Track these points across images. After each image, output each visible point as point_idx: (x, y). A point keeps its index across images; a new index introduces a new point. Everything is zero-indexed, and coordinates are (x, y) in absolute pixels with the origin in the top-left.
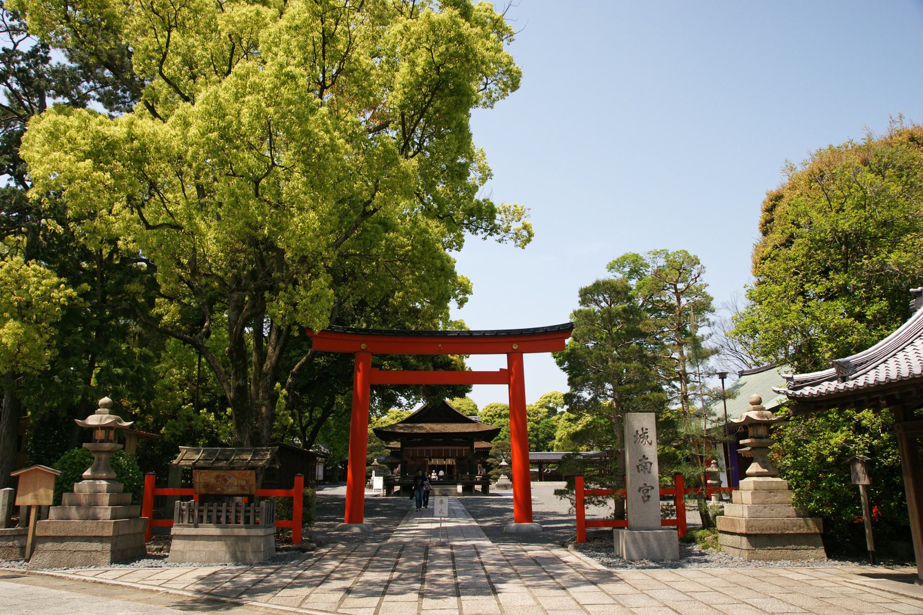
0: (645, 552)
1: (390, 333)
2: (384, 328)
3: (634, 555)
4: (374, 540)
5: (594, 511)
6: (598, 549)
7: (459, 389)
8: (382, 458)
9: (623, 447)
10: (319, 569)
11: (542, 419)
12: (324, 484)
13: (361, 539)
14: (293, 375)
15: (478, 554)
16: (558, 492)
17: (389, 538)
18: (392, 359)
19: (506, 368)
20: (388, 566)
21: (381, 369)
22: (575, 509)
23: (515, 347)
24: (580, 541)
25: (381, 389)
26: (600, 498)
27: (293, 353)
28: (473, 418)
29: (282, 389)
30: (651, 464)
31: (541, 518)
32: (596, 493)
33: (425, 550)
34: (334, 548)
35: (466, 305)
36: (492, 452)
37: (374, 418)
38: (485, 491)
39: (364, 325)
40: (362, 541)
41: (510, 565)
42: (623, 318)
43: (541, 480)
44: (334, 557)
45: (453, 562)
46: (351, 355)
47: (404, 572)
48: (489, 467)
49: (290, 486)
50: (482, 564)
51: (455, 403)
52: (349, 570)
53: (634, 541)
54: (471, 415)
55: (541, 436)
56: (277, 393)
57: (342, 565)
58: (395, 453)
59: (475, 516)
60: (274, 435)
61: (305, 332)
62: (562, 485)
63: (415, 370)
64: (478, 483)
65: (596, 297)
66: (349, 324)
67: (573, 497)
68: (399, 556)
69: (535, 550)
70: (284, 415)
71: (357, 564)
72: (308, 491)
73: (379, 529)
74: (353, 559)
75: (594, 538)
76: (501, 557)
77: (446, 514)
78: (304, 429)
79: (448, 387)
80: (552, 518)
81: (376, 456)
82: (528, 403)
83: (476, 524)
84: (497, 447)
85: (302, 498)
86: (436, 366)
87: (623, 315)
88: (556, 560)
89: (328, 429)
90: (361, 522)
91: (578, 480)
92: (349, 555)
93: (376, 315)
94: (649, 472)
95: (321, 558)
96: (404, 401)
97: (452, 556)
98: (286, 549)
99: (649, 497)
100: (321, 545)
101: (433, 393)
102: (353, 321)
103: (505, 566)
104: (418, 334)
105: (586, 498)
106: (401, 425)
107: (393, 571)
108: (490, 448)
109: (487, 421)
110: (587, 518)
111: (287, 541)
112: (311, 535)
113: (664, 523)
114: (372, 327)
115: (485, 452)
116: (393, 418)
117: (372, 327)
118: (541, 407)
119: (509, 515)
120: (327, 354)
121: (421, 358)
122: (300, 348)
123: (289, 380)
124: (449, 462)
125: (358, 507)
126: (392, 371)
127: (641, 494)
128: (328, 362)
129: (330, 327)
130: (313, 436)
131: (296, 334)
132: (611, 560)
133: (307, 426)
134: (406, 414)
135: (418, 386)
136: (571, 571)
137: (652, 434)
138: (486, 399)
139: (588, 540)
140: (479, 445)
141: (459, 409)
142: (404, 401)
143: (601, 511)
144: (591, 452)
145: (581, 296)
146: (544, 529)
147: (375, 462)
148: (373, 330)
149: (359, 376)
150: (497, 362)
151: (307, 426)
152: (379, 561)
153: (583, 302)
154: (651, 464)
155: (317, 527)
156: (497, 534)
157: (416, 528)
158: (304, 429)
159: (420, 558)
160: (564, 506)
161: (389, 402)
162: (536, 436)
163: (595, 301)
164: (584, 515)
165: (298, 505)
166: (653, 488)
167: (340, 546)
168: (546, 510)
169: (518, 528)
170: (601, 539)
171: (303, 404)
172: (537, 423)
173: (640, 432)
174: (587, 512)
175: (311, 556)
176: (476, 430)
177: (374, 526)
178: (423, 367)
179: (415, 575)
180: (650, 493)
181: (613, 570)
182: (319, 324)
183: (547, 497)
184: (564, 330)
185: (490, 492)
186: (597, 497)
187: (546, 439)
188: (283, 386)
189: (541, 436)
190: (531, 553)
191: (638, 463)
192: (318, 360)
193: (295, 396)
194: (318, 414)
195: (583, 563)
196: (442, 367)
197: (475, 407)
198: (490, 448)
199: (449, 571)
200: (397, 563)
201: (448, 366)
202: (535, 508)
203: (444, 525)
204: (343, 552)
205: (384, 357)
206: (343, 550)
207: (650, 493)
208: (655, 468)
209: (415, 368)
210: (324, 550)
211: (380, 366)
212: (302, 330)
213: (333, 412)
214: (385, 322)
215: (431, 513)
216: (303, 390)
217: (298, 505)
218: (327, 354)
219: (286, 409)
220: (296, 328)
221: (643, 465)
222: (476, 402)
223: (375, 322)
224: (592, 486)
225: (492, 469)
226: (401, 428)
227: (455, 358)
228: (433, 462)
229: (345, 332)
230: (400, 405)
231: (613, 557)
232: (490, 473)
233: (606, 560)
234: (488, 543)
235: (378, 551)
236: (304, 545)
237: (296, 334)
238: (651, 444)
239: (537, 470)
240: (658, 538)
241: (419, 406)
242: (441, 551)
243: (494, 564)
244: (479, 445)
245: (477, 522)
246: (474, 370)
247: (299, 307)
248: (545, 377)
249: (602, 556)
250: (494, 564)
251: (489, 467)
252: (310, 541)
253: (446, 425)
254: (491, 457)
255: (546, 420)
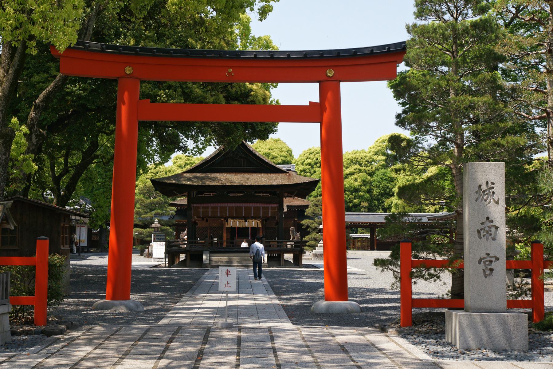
0: (485, 339)
1: (167, 52)
2: (159, 46)
3: (472, 343)
4: (144, 321)
5: (422, 288)
6: (427, 335)
7: (259, 128)
8: (166, 218)
9: (462, 207)
10: (66, 356)
11: (377, 169)
12: (88, 252)
13: (127, 320)
14: (37, 107)
15: (272, 339)
16: (379, 263)
17: (161, 318)
18: (169, 87)
19: (318, 101)
20: (156, 352)
21: (154, 101)
22: (399, 284)
23: (330, 73)
24: (404, 325)
25: (159, 127)
26: (432, 271)
27: (36, 78)
28: (284, 167)
29: (20, 125)
30: (497, 228)
31: (362, 296)
32: (429, 264)
33: (206, 333)
34: (89, 330)
35: (270, 16)
36: (308, 211)
37: (151, 165)
38: (297, 261)
39: (132, 42)
40: (128, 323)
41: (310, 353)
42: (473, 36)
43: (372, 249)
44: (89, 342)
45: (239, 348)
46: (115, 81)
47: (175, 359)
48: (304, 231)
49: (32, 253)
50: (274, 350)
51: (257, 146)
52: (104, 358)
53: (473, 325)
54: (284, 162)
55: (375, 192)
56: (13, 132)
57: (98, 351)
58: (181, 211)
59: (278, 292)
60: (13, 187)
61: (46, 48)
62: (385, 255)
63: (201, 102)
64: (288, 252)
65: (437, 7)
66: (111, 41)
67: (398, 269)
68: (171, 340)
69: (347, 335)
70: (24, 160)
71: (117, 350)
72: (56, 258)
73: (151, 307)
74: (113, 344)
75: (422, 321)
76: (301, 342)
77: (234, 288)
78: (57, 180)
79: (245, 125)
80: (376, 296)
81: (156, 215)
82: (344, 151)
83: (277, 302)
84: (316, 205)
85: (47, 268)
86: (229, 99)
87: (473, 32)
88: (371, 347)
89: (89, 179)
90: (128, 298)
91: (404, 247)
92: (107, 339)
93: (148, 27)
94: (494, 239)
95: (71, 343)
96: (190, 144)
97: (239, 341)
98: (27, 333)
99: (492, 270)
100: (73, 327)
101: (222, 132)
102: (118, 35)
103: (305, 353)
104: (203, 54)
105: (414, 270)
106: (189, 175)
107: (160, 358)
108: (307, 207)
109: (304, 171)
110: (413, 296)
111: (29, 322)
112: (61, 314)
113: (512, 304)
114: (142, 44)
115: (300, 212)
116: (180, 166)
117: (142, 44)
118: (377, 153)
119: (321, 292)
120: (84, 80)
121: (214, 86)
122: (47, 71)
123: (32, 114)
124: (253, 223)
125: (125, 281)
126: (170, 105)
127: (482, 266)
128: (84, 90)
129: (78, 43)
130: (71, 188)
131: (34, 52)
132: (439, 348)
133: (61, 175)
134: (197, 159)
135: (206, 124)
136: (387, 360)
137: (500, 191)
138: (296, 142)
139: (414, 324)
140: (289, 202)
141: (267, 155)
142: (190, 144)
143: (434, 287)
144: (440, 214)
145: (417, 5)
146: (362, 309)
147: (156, 224)
148: (142, 49)
149: (124, 110)
150: (305, 93)
151: (61, 175)
152: (144, 346)
153: (420, 14)
154: (497, 228)
155: (69, 303)
156: (300, 315)
157: (199, 307)
158: (57, 180)
159: (198, 343)
160: (386, 280)
161: (170, 145)
162: (369, 191)
163: (436, 11)
164: (411, 292)
165: (42, 275)
166: (497, 259)
167: (98, 328)
168: (372, 286)
169: (328, 307)
170: (432, 322)
171: (54, 146)
172: (371, 174)
173: (484, 187)
174: (414, 288)
175: (58, 341)
176: (286, 183)
177: (145, 304)
178: (212, 99)
179: (188, 362)
180: (493, 266)
181: (441, 360)
182: (64, 39)
183: (367, 270)
184: (396, 52)
185: (304, 262)
186: (430, 269)
187: (382, 195)
188: (22, 121)
189: (375, 192)
190: (340, 339)
191: (480, 227)
192: (69, 87)
193: (39, 136)
194: (76, 159)
195: (404, 352)
196: (237, 99)
197: (289, 152)
198: (307, 207)
199: (232, 359)
200: (167, 349)
201: (245, 97)
202: (352, 283)
203: (230, 303)
204: (101, 336)
205: (159, 84)
206: (101, 333)
207: (493, 266)
208: (503, 231)
209: (201, 101)
210: (75, 334)
211: (153, 98)
212: (40, 44)
213: (97, 157)
214: (160, 37)
215: (213, 288)
216: (52, 128)
217: (42, 275)
218: (84, 80)
219: (26, 153)
220: (34, 43)
221: (487, 229)
222: (291, 146)
223: (147, 37)
224: (423, 255)
225: (308, 233)
226: (189, 179)
227: (254, 87)
228: (231, 223)
229: (103, 51)
230: (185, 149)
231: (444, 345)
232: (306, 238)
233: (433, 348)
234: (288, 325)
235: (144, 334)
236: (51, 327)
237: (34, 52)
238: (497, 203)
239: (368, 236)
240: (503, 323)
241: (210, 151)
242: (227, 334)
243: (290, 351)
244: (289, 202)
245: (280, 299)
246: (283, 103)
247: (36, 16)
248: (370, 114)
249: (430, 343)
250: (290, 351)
251: (304, 231)
252: (58, 323)
253: (247, 176)
254: (308, 217)
255: (383, 171)
